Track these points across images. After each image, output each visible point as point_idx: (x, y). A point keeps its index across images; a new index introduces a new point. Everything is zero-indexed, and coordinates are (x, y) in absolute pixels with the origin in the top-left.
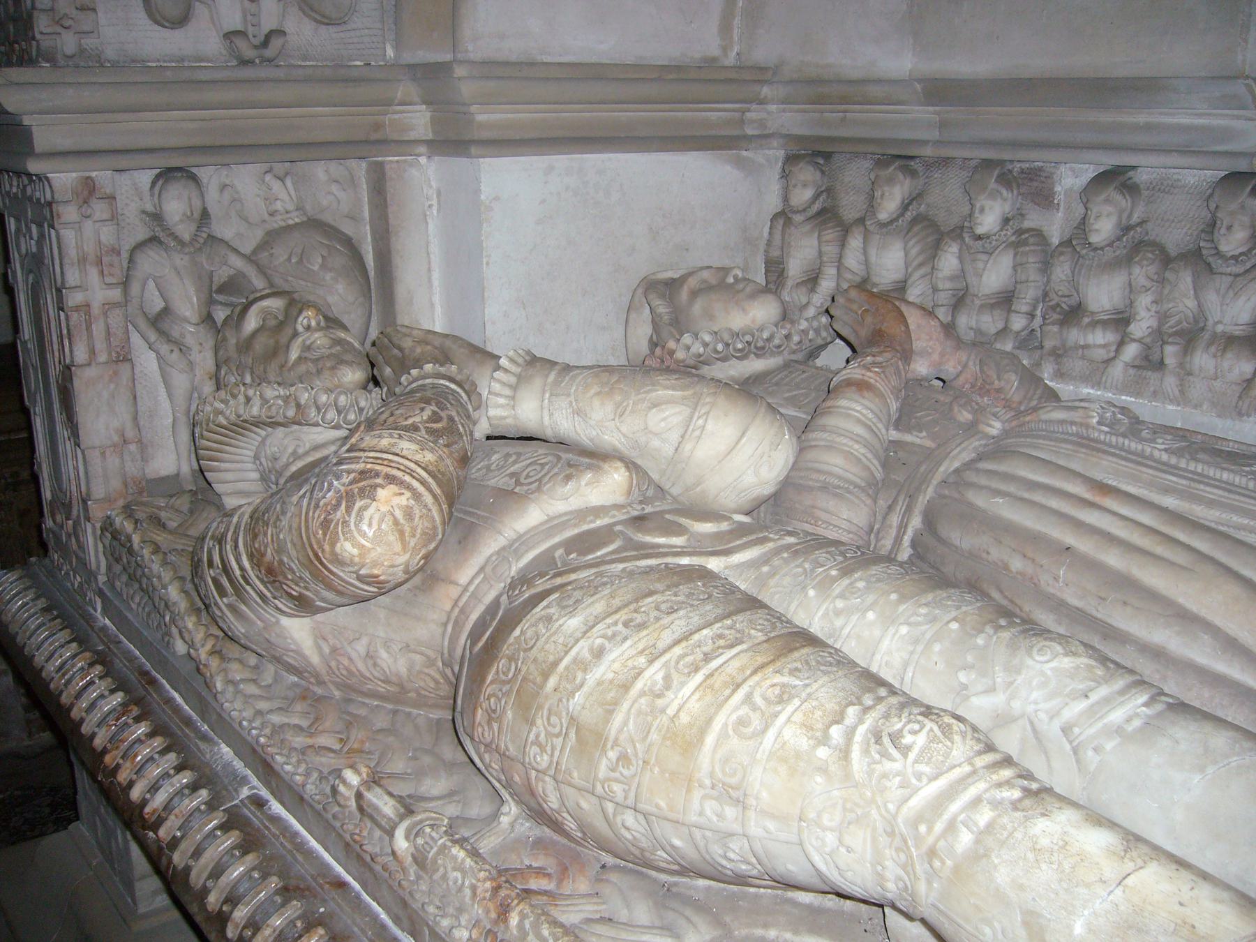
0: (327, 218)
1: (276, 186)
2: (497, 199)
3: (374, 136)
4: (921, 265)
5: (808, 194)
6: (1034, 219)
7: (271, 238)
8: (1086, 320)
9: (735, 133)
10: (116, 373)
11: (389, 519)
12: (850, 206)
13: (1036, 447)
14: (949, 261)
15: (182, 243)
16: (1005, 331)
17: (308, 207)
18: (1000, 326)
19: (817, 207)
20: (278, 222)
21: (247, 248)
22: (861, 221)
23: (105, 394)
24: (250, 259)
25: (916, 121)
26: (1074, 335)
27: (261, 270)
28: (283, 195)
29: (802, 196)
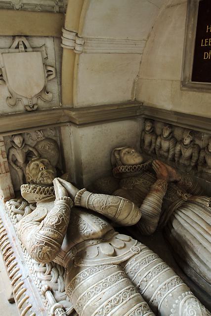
0: (50, 137)
1: (39, 133)
2: (83, 135)
3: (58, 122)
4: (172, 148)
5: (149, 128)
6: (197, 142)
7: (38, 143)
8: (207, 167)
9: (134, 115)
10: (7, 175)
11: (46, 254)
12: (158, 131)
13: (194, 209)
14: (178, 148)
15: (19, 148)
16: (190, 165)
17: (46, 136)
18: (189, 164)
19: (151, 131)
20: (39, 139)
21: (33, 145)
22: (160, 135)
23: (5, 179)
24: (34, 148)
25: (174, 119)
26: (204, 170)
27: (36, 150)
28: (40, 134)
29: (148, 128)
